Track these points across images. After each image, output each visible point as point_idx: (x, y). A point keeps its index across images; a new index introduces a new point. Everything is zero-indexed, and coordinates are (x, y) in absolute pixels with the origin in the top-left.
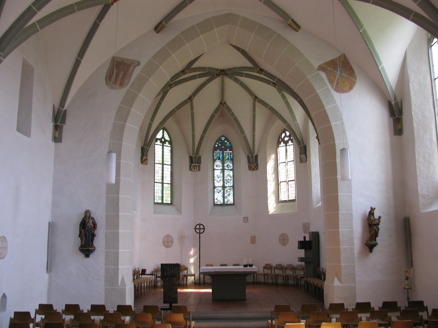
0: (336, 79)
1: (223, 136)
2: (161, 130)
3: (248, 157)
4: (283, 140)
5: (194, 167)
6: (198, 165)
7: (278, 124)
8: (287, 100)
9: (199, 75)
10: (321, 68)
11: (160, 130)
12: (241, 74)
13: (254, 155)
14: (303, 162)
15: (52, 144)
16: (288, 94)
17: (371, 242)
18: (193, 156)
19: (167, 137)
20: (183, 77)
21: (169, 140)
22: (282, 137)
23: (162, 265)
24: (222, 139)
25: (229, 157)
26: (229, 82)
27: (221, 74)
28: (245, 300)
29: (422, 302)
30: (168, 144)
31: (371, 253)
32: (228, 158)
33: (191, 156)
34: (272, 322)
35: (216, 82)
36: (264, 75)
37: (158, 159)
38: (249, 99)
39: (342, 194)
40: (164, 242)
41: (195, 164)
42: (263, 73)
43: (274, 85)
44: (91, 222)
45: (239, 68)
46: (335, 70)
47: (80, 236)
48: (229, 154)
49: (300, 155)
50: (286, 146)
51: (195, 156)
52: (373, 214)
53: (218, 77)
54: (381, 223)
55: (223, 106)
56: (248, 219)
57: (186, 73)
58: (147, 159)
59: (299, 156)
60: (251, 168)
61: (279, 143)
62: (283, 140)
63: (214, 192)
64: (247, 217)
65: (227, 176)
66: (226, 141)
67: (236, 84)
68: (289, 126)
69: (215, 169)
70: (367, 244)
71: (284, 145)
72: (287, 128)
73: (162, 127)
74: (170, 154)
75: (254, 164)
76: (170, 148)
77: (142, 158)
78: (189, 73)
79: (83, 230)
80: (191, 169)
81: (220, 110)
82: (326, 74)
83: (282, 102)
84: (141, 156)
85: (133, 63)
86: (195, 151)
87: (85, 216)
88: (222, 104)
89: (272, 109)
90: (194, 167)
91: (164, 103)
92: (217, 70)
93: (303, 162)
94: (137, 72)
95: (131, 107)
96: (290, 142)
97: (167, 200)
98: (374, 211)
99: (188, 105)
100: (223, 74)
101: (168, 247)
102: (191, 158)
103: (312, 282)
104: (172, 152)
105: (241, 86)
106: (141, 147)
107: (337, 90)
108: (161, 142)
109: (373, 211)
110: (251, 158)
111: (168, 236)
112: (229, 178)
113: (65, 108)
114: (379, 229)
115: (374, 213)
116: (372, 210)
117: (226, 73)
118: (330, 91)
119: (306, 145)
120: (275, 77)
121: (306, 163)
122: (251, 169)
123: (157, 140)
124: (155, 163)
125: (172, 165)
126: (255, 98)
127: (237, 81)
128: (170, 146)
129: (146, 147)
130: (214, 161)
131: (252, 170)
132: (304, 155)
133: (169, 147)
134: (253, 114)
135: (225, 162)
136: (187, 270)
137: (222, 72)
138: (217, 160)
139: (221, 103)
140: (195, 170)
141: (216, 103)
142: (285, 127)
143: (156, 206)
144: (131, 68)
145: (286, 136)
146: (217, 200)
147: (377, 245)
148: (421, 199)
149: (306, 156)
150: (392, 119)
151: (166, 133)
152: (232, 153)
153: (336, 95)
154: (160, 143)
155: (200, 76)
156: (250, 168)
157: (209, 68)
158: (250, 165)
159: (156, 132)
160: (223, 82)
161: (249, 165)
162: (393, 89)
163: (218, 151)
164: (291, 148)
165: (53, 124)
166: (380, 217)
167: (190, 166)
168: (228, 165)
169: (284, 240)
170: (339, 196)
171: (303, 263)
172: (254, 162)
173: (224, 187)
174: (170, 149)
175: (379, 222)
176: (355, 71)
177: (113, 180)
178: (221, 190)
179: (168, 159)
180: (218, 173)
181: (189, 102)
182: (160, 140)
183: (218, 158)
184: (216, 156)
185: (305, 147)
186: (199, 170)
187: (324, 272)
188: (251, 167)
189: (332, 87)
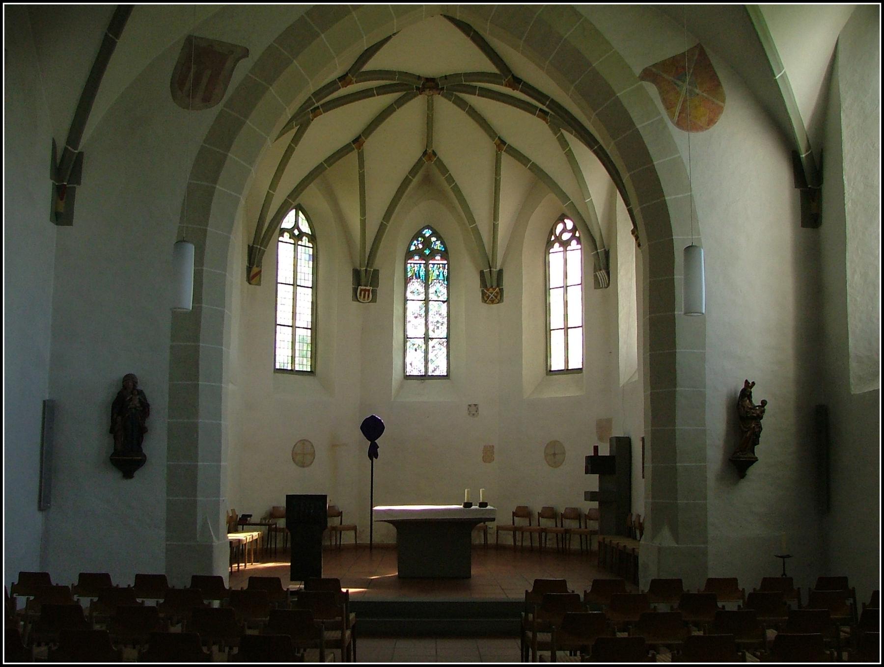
0: (681, 99)
1: (428, 227)
2: (292, 209)
3: (482, 273)
4: (560, 238)
5: (363, 293)
6: (371, 288)
7: (547, 204)
8: (570, 150)
9: (378, 88)
10: (649, 75)
11: (290, 211)
12: (472, 90)
13: (495, 270)
15: (52, 229)
16: (575, 136)
17: (742, 455)
18: (362, 269)
19: (305, 227)
20: (343, 91)
21: (310, 233)
22: (558, 233)
23: (289, 498)
24: (425, 234)
25: (440, 273)
26: (444, 106)
27: (427, 88)
28: (470, 577)
29: (845, 580)
30: (307, 242)
31: (742, 480)
32: (439, 276)
33: (357, 270)
34: (526, 615)
35: (417, 104)
36: (522, 91)
37: (285, 273)
38: (487, 146)
39: (682, 351)
40: (294, 454)
41: (364, 288)
42: (520, 86)
43: (543, 114)
44: (136, 402)
45: (466, 74)
46: (679, 79)
47: (112, 430)
48: (440, 267)
49: (595, 271)
50: (565, 250)
51: (366, 270)
52: (750, 396)
53: (420, 94)
54: (765, 416)
55: (430, 159)
56: (477, 408)
57: (350, 83)
59: (593, 274)
60: (488, 297)
61: (549, 245)
62: (558, 239)
63: (405, 351)
64: (475, 405)
65: (435, 313)
66: (433, 239)
67: (459, 110)
68: (573, 206)
69: (408, 300)
70: (734, 459)
71: (562, 249)
72: (568, 213)
73: (295, 204)
74: (311, 263)
75: (494, 289)
76: (311, 250)
77: (249, 269)
78: (356, 82)
79: (119, 418)
80: (355, 298)
81: (423, 169)
83: (560, 153)
84: (247, 266)
87: (125, 387)
88: (429, 154)
89: (537, 171)
90: (363, 293)
91: (299, 149)
92: (419, 77)
94: (242, 71)
95: (228, 148)
96: (574, 242)
97: (303, 364)
98: (752, 390)
99: (354, 155)
100: (431, 88)
101: (303, 467)
102: (356, 273)
103: (615, 542)
104: (315, 258)
106: (249, 246)
107: (679, 124)
108: (292, 236)
109: (749, 389)
110: (487, 276)
111: (303, 442)
112: (438, 318)
113: (80, 148)
114: (761, 428)
115: (751, 392)
116: (749, 386)
118: (666, 127)
119: (609, 250)
120: (547, 97)
121: (608, 288)
122: (486, 301)
123: (282, 231)
124: (277, 283)
125: (315, 287)
126: (501, 144)
127: (462, 104)
128: (311, 245)
129: (259, 247)
130: (407, 281)
131: (491, 302)
132: (603, 272)
133: (309, 247)
134: (496, 178)
136: (340, 517)
138: (413, 279)
139: (425, 153)
140: (365, 300)
141: (416, 153)
142: (564, 208)
143: (279, 375)
144: (229, 64)
146: (413, 365)
147: (757, 462)
148: (853, 365)
149: (608, 274)
150: (798, 191)
151: (304, 218)
152: (446, 265)
153: (678, 135)
154: (290, 238)
155: (382, 90)
156: (485, 298)
157: (400, 73)
158: (485, 290)
159: (281, 214)
160: (430, 107)
161: (483, 291)
162: (803, 126)
164: (575, 255)
165: (53, 183)
166: (764, 403)
167: (355, 290)
168: (438, 291)
169: (554, 454)
170: (678, 356)
171: (595, 505)
172: (495, 284)
173: (427, 338)
174: (311, 253)
175: (763, 412)
176: (723, 85)
177: (189, 304)
178: (421, 345)
180: (414, 307)
181: (356, 150)
182: (291, 231)
183: (416, 274)
184: (413, 271)
185: (607, 254)
186: (374, 300)
187: (641, 523)
189: (672, 117)
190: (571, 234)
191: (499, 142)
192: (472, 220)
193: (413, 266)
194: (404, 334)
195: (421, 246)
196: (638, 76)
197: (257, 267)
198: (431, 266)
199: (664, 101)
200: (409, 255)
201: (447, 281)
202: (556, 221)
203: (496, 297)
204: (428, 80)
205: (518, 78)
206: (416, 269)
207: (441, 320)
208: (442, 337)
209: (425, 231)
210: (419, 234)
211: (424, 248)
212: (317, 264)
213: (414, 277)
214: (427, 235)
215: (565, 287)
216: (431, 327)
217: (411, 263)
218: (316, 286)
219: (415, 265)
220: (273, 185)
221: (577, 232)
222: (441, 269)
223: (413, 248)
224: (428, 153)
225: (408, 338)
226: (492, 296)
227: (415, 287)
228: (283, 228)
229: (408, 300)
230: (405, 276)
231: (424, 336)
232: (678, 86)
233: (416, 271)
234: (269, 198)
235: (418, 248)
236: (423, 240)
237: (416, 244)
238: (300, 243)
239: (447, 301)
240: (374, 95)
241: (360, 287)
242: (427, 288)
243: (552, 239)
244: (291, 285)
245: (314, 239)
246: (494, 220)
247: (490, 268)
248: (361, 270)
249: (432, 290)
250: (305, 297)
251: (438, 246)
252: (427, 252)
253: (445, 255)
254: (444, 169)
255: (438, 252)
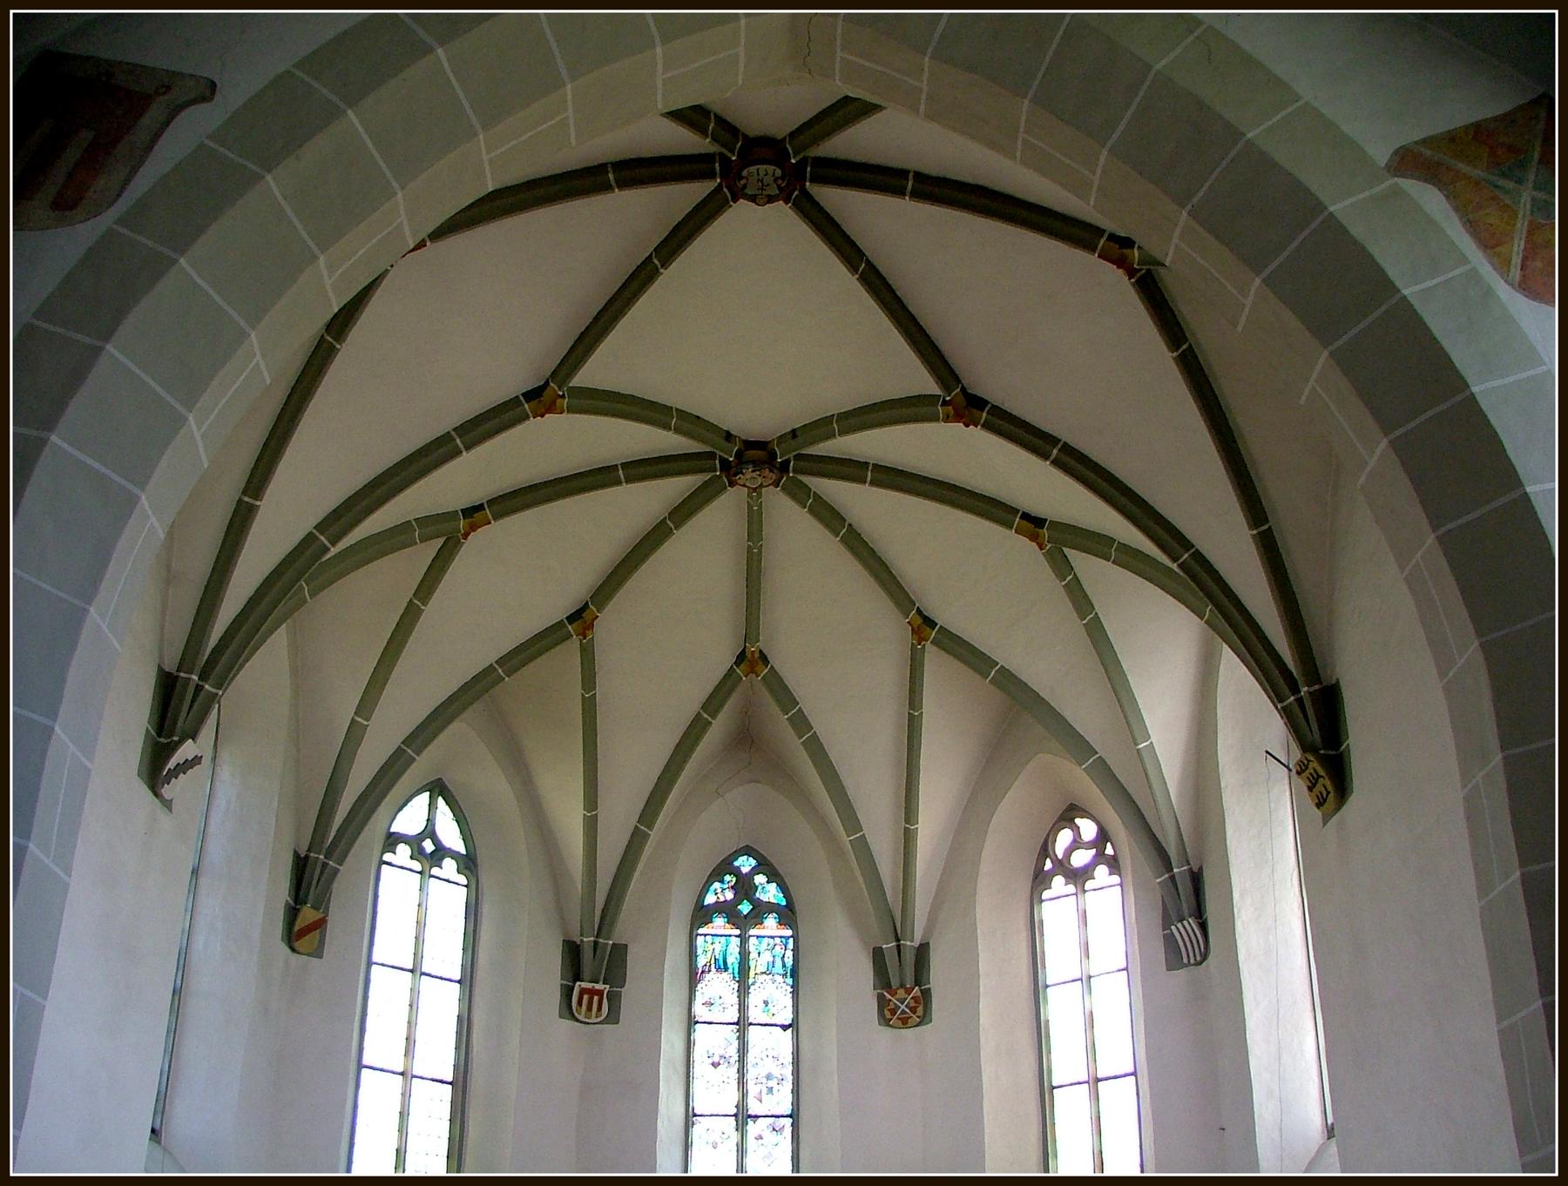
1: (748, 851)
3: (878, 955)
10: (1409, 162)
13: (908, 943)
14: (1185, 961)
19: (450, 833)
21: (465, 853)
22: (1060, 854)
25: (774, 956)
33: (575, 942)
35: (725, 511)
38: (891, 630)
41: (589, 985)
49: (1167, 923)
51: (596, 943)
58: (320, 924)
60: (893, 1012)
61: (1040, 880)
62: (1062, 867)
68: (1105, 774)
69: (697, 1022)
71: (1071, 888)
75: (909, 991)
77: (292, 913)
80: (568, 1011)
81: (739, 689)
82: (1447, 197)
85: (169, 88)
86: (598, 913)
88: (751, 660)
89: (1009, 683)
90: (586, 997)
92: (728, 436)
93: (1185, 961)
96: (1102, 871)
99: (568, 654)
100: (757, 464)
102: (572, 952)
105: (851, 548)
108: (419, 853)
110: (891, 961)
117: (773, 455)
118: (1488, 293)
119: (1201, 869)
123: (392, 841)
125: (467, 981)
126: (924, 625)
130: (694, 977)
135: (753, 984)
137: (752, 453)
139: (741, 658)
141: (721, 659)
145: (1077, 844)
149: (1203, 927)
156: (888, 1014)
161: (881, 998)
163: (719, 922)
167: (567, 992)
179: (446, 953)
180: (713, 1041)
182: (415, 842)
184: (709, 954)
185: (1196, 879)
186: (613, 1017)
188: (892, 1006)
189: (1503, 266)
190: (1093, 851)
191: (919, 621)
192: (852, 821)
193: (710, 942)
194: (687, 1104)
195: (729, 895)
196: (1383, 165)
197: (316, 908)
198: (753, 941)
199: (1472, 226)
200: (702, 914)
201: (792, 976)
202: (1054, 824)
203: (913, 1010)
204: (749, 445)
205: (975, 397)
206: (718, 948)
207: (776, 1072)
208: (779, 1114)
209: (741, 859)
210: (724, 867)
211: (737, 901)
212: (475, 926)
213: (713, 966)
214: (745, 870)
215: (1086, 980)
216: (752, 1089)
217: (705, 935)
218: (472, 977)
219: (717, 939)
220: (367, 705)
221: (1109, 845)
222: (778, 948)
223: (710, 899)
224: (749, 655)
225: (695, 1115)
226: (903, 1007)
227: (717, 989)
228: (394, 833)
229: (697, 1022)
230: (691, 965)
231: (734, 1111)
232: (1507, 192)
233: (717, 953)
234: (355, 734)
235: (722, 899)
236: (734, 879)
237: (719, 891)
238: (435, 871)
239: (793, 1026)
240: (619, 483)
241: (578, 983)
242: (743, 989)
243: (1046, 868)
244: (409, 970)
245: (473, 867)
246: (907, 820)
247: (898, 940)
248: (582, 940)
249: (755, 998)
250: (442, 1004)
251: (770, 893)
252: (745, 908)
253: (787, 915)
254: (784, 696)
255: (771, 908)
